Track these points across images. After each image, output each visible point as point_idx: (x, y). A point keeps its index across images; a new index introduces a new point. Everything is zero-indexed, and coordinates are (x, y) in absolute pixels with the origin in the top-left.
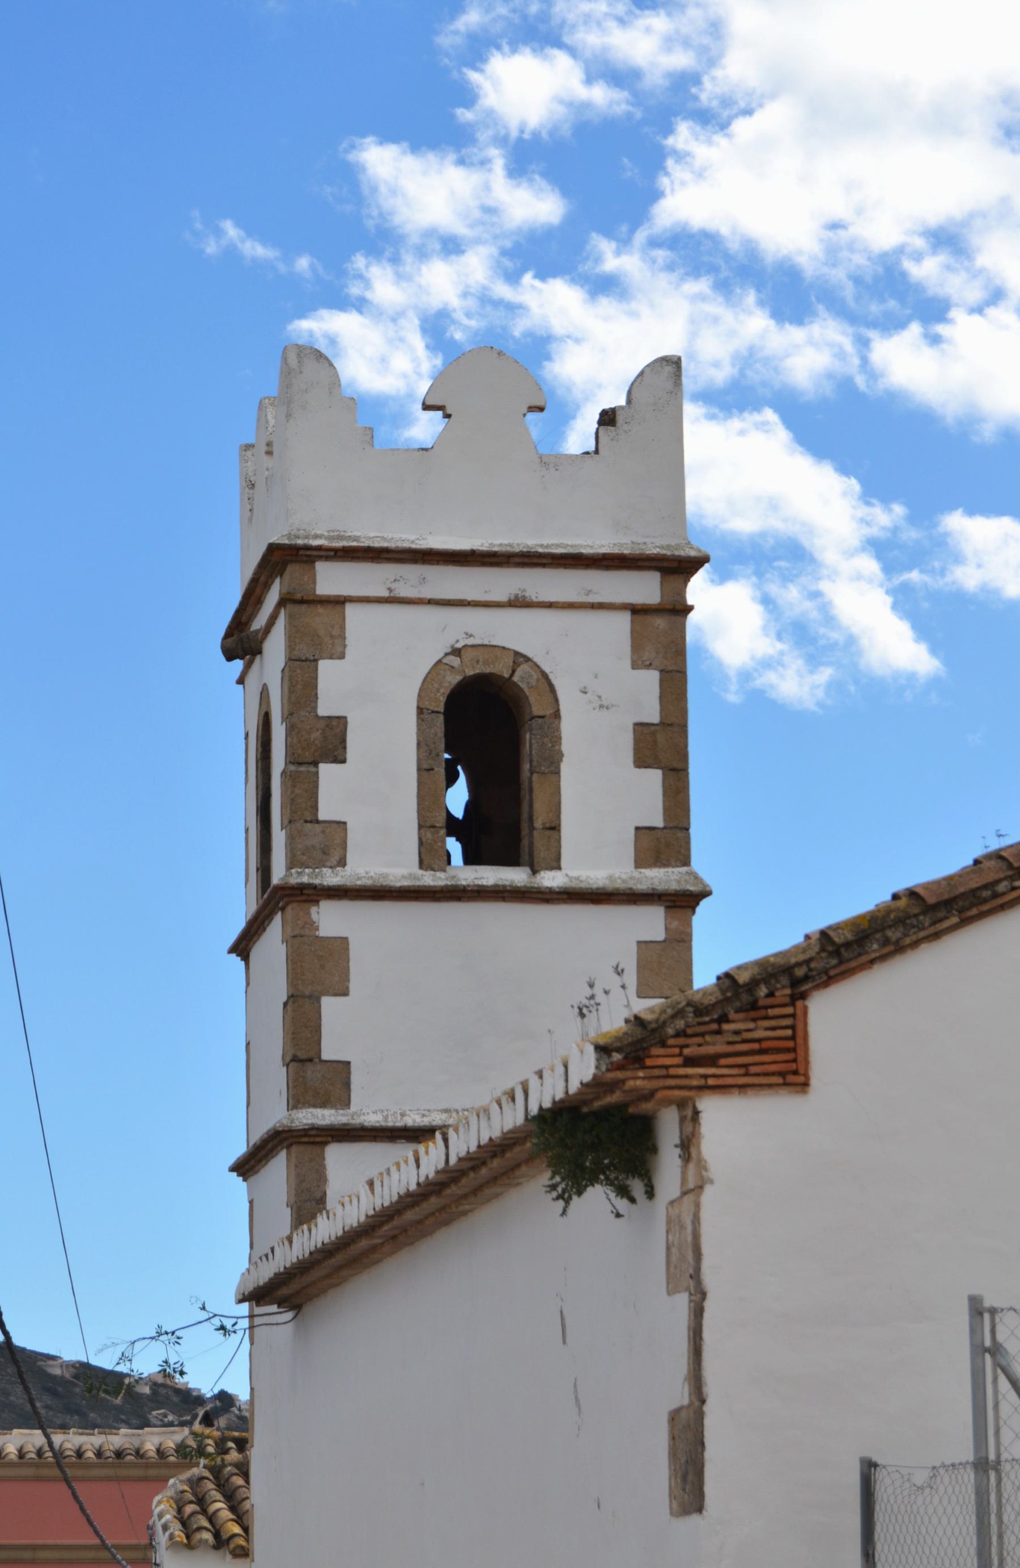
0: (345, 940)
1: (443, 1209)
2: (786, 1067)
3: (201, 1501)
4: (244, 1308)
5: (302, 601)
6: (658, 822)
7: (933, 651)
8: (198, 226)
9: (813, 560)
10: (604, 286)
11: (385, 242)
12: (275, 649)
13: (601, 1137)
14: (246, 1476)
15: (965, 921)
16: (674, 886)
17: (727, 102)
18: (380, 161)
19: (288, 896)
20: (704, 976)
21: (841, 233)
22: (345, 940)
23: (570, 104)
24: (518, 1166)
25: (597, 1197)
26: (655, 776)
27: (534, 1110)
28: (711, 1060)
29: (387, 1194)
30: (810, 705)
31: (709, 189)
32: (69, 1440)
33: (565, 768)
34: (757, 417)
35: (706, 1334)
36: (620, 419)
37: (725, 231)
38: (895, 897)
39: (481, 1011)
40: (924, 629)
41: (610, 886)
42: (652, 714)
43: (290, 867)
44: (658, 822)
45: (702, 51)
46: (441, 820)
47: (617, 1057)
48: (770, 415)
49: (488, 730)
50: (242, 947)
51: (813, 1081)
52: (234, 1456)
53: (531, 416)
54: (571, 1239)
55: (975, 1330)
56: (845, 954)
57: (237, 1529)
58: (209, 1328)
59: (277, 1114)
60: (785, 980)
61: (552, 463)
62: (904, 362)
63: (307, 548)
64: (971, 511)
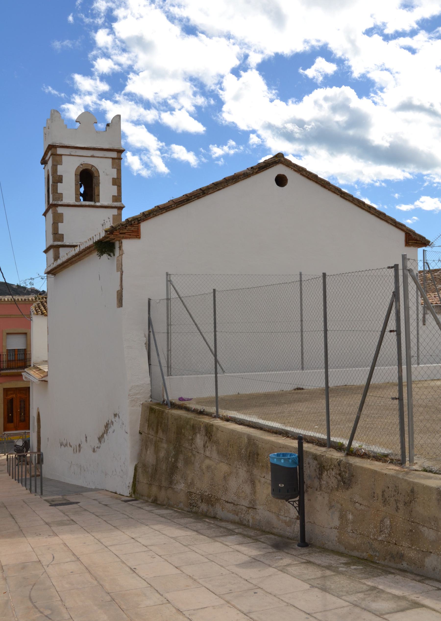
1: (79, 258)
2: (136, 234)
3: (39, 307)
4: (46, 275)
5: (55, 155)
6: (116, 195)
7: (169, 168)
8: (44, 87)
9: (149, 151)
10: (116, 102)
11: (77, 91)
12: (50, 163)
13: (106, 246)
14: (46, 303)
15: (167, 211)
16: (119, 206)
17: (138, 70)
18: (78, 78)
19: (53, 206)
20: (124, 219)
21: (157, 95)
23: (111, 69)
25: (105, 256)
26: (116, 187)
27: (94, 241)
28: (124, 233)
29: (70, 255)
30: (147, 177)
31: (134, 85)
32: (16, 297)
33: (100, 185)
34: (141, 126)
36: (110, 125)
37: (137, 93)
38: (155, 207)
39: (86, 225)
40: (167, 164)
41: (108, 205)
43: (53, 201)
44: (116, 195)
45: (133, 61)
46: (79, 194)
48: (143, 126)
49: (87, 179)
50: (45, 214)
51: (141, 237)
52: (45, 300)
53: (95, 124)
54: (100, 263)
55: (167, 278)
56: (147, 216)
57: (45, 312)
58: (40, 278)
59: (51, 242)
60: (137, 220)
61: (98, 132)
62: (167, 119)
63: (55, 145)
64: (176, 144)
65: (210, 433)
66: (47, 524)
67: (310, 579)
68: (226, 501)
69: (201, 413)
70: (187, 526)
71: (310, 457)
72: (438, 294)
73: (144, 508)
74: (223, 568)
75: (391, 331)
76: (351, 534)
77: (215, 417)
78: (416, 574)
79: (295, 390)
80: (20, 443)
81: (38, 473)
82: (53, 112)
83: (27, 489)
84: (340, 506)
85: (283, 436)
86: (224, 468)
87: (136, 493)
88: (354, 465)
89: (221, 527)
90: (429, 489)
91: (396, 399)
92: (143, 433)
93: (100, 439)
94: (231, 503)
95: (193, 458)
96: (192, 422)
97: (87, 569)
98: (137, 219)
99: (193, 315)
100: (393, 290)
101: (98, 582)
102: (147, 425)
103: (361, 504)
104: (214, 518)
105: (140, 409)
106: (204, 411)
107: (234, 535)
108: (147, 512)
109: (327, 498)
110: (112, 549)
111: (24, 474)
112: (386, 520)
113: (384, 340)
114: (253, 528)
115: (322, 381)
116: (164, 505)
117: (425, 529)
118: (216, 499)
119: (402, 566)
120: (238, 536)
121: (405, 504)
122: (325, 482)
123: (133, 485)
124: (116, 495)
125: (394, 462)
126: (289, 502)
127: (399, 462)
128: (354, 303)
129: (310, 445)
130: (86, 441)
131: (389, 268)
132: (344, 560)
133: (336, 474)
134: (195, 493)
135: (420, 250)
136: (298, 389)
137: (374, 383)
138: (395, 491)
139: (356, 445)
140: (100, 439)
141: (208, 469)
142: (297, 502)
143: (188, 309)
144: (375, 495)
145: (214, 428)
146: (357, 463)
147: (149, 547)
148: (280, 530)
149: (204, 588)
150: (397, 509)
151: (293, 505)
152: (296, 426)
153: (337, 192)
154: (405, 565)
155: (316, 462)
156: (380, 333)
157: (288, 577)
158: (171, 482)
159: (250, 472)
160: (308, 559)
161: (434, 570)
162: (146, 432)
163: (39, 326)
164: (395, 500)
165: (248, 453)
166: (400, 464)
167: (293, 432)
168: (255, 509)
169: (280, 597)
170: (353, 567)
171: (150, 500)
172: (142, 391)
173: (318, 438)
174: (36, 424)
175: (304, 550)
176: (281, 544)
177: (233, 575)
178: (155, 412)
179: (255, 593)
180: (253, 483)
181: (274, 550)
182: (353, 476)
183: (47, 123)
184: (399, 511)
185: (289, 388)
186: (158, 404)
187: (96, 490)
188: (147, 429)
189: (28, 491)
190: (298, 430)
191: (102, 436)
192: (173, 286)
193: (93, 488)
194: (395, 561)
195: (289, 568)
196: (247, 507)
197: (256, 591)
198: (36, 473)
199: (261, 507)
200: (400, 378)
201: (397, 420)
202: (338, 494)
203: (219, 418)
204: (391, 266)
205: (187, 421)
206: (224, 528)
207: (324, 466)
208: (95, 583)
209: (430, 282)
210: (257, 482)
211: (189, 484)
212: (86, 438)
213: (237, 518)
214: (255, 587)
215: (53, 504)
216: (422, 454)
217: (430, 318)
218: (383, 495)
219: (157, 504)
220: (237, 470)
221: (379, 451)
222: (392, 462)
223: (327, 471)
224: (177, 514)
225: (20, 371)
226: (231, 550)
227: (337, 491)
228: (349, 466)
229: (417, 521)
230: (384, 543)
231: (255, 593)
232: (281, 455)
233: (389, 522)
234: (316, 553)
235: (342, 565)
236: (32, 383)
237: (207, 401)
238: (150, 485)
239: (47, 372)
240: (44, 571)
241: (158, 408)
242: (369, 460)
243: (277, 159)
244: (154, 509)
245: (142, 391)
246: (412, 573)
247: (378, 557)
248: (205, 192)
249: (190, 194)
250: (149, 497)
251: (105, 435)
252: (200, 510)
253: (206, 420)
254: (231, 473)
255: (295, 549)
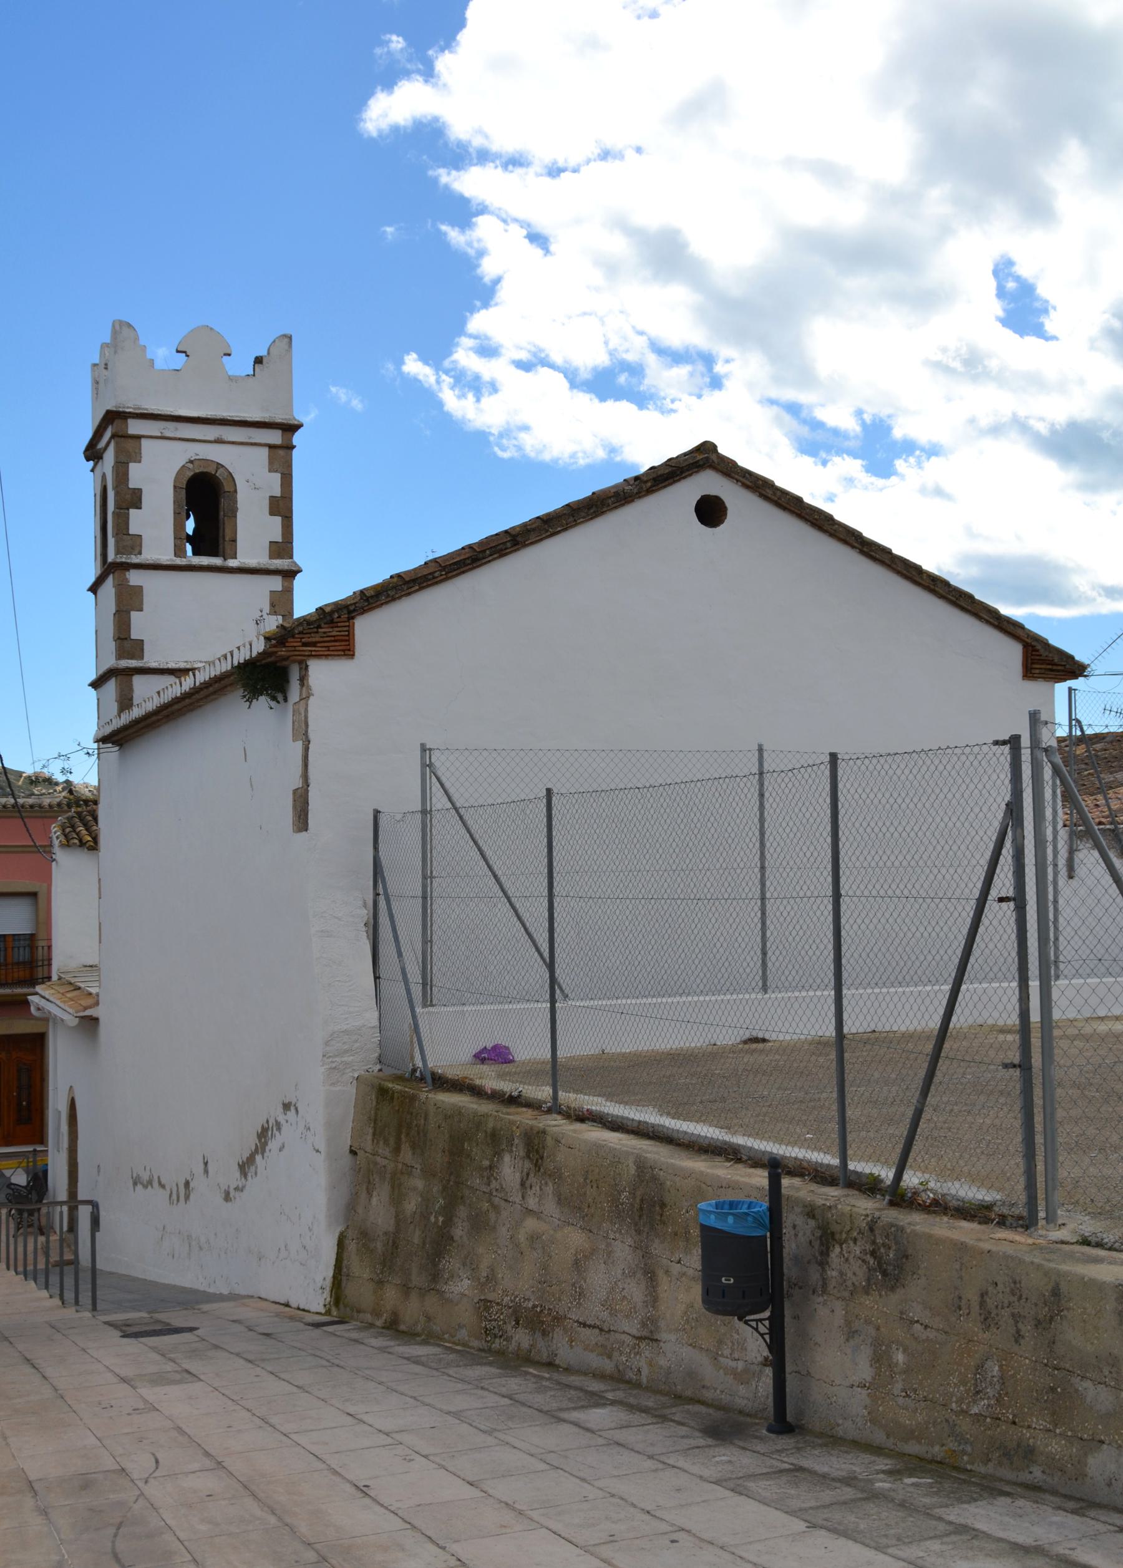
0: (141, 587)
1: (191, 704)
2: (344, 648)
3: (73, 827)
12: (109, 457)
13: (267, 674)
15: (421, 588)
16: (286, 568)
22: (141, 587)
24: (226, 687)
25: (263, 700)
26: (278, 519)
27: (236, 663)
28: (314, 644)
29: (167, 697)
33: (239, 515)
35: (310, 758)
36: (265, 361)
38: (392, 577)
39: (206, 621)
41: (258, 567)
42: (277, 492)
46: (184, 536)
47: (274, 642)
49: (205, 500)
50: (94, 589)
55: (423, 758)
58: (82, 753)
59: (111, 662)
60: (345, 611)
65: (537, 1152)
66: (124, 1380)
67: (806, 1510)
68: (580, 1323)
69: (513, 1101)
70: (485, 1384)
71: (798, 1210)
72: (1106, 799)
73: (366, 1341)
74: (585, 1485)
75: (1001, 900)
76: (901, 1400)
77: (549, 1111)
78: (1065, 1496)
79: (745, 1042)
80: (20, 1179)
81: (68, 1256)
82: (117, 327)
83: (51, 1297)
84: (872, 1331)
85: (728, 1160)
86: (575, 1238)
87: (341, 1306)
88: (908, 1231)
89: (569, 1387)
90: (1096, 1287)
91: (1015, 1066)
92: (360, 1153)
93: (245, 1167)
94: (594, 1327)
95: (492, 1216)
96: (490, 1125)
97: (245, 1487)
98: (347, 607)
99: (489, 853)
100: (1008, 798)
101: (280, 1519)
102: (371, 1131)
103: (926, 1327)
104: (550, 1365)
105: (352, 1090)
106: (519, 1096)
107: (604, 1405)
108: (376, 1351)
109: (840, 1312)
110: (302, 1439)
111: (30, 1257)
112: (989, 1363)
113: (985, 921)
114: (651, 1389)
115: (827, 1021)
116: (418, 1335)
117: (1088, 1384)
118: (555, 1318)
119: (1029, 1477)
120: (615, 1409)
121: (1038, 1323)
122: (834, 1274)
123: (333, 1283)
124: (287, 1309)
125: (1008, 1223)
126: (746, 1323)
127: (1021, 1222)
128: (943, 842)
129: (796, 1181)
130: (206, 1171)
131: (996, 743)
132: (884, 1464)
133: (864, 1252)
134: (498, 1304)
135: (1061, 689)
136: (756, 1040)
137: (958, 1026)
138: (1013, 1293)
139: (911, 1179)
140: (245, 1167)
141: (530, 1239)
142: (767, 1323)
143: (477, 837)
144: (963, 1302)
145: (549, 1138)
146: (918, 1224)
147: (394, 1435)
148: (722, 1392)
149: (544, 1530)
150: (1018, 1337)
151: (756, 1329)
152: (757, 1135)
153: (852, 540)
154: (1037, 1474)
155: (812, 1223)
156: (973, 903)
157: (751, 1506)
158: (435, 1277)
159: (642, 1250)
160: (795, 1462)
161: (1109, 1485)
162: (369, 1148)
163: (71, 878)
164: (1013, 1315)
165: (638, 1201)
166: (1022, 1226)
167: (751, 1149)
168: (657, 1340)
169: (736, 1551)
170: (909, 1481)
171: (379, 1323)
172: (357, 1045)
173: (817, 1163)
174: (65, 1128)
175: (785, 1442)
176: (724, 1427)
177: (612, 1500)
178: (392, 1098)
179: (673, 1541)
180: (650, 1275)
181: (710, 1441)
182: (907, 1257)
183: (102, 354)
184: (1022, 1342)
185: (728, 1037)
186: (399, 1078)
187: (233, 1297)
188: (370, 1142)
189: (57, 1301)
190: (765, 1143)
191: (251, 1160)
192: (438, 779)
193: (225, 1292)
194: (1012, 1463)
195: (751, 1485)
196: (634, 1337)
197: (674, 1536)
198: (62, 1254)
199: (673, 1337)
200: (1024, 1014)
201: (1016, 1122)
202: (867, 1301)
203: (559, 1113)
204: (1001, 738)
205: (478, 1121)
206: (576, 1388)
207: (833, 1234)
208: (273, 1520)
209: (1083, 766)
210: (660, 1274)
211: (483, 1280)
212: (206, 1164)
213: (608, 1366)
214: (671, 1529)
215: (130, 1332)
216: (1077, 1202)
217: (1089, 859)
218: (982, 1304)
219: (397, 1331)
220: (608, 1245)
221: (970, 1195)
222: (1002, 1221)
223: (841, 1245)
224: (452, 1356)
225: (25, 990)
226: (601, 1441)
227: (867, 1293)
228: (896, 1232)
229: (1067, 1366)
230: (985, 1421)
231: (673, 1541)
232: (726, 1206)
233: (997, 1368)
234: (813, 1447)
235: (881, 1476)
236: (55, 1023)
237: (532, 1073)
238: (380, 1283)
239: (98, 995)
240: (138, 1493)
241: (399, 1087)
242: (945, 1219)
243: (699, 457)
244: (392, 1343)
245: (357, 1045)
246: (1054, 1492)
247: (969, 1455)
248: (519, 539)
249: (481, 543)
250: (377, 1313)
251: (258, 1158)
252: (513, 1346)
253: (524, 1118)
254: (593, 1251)
255: (760, 1438)
